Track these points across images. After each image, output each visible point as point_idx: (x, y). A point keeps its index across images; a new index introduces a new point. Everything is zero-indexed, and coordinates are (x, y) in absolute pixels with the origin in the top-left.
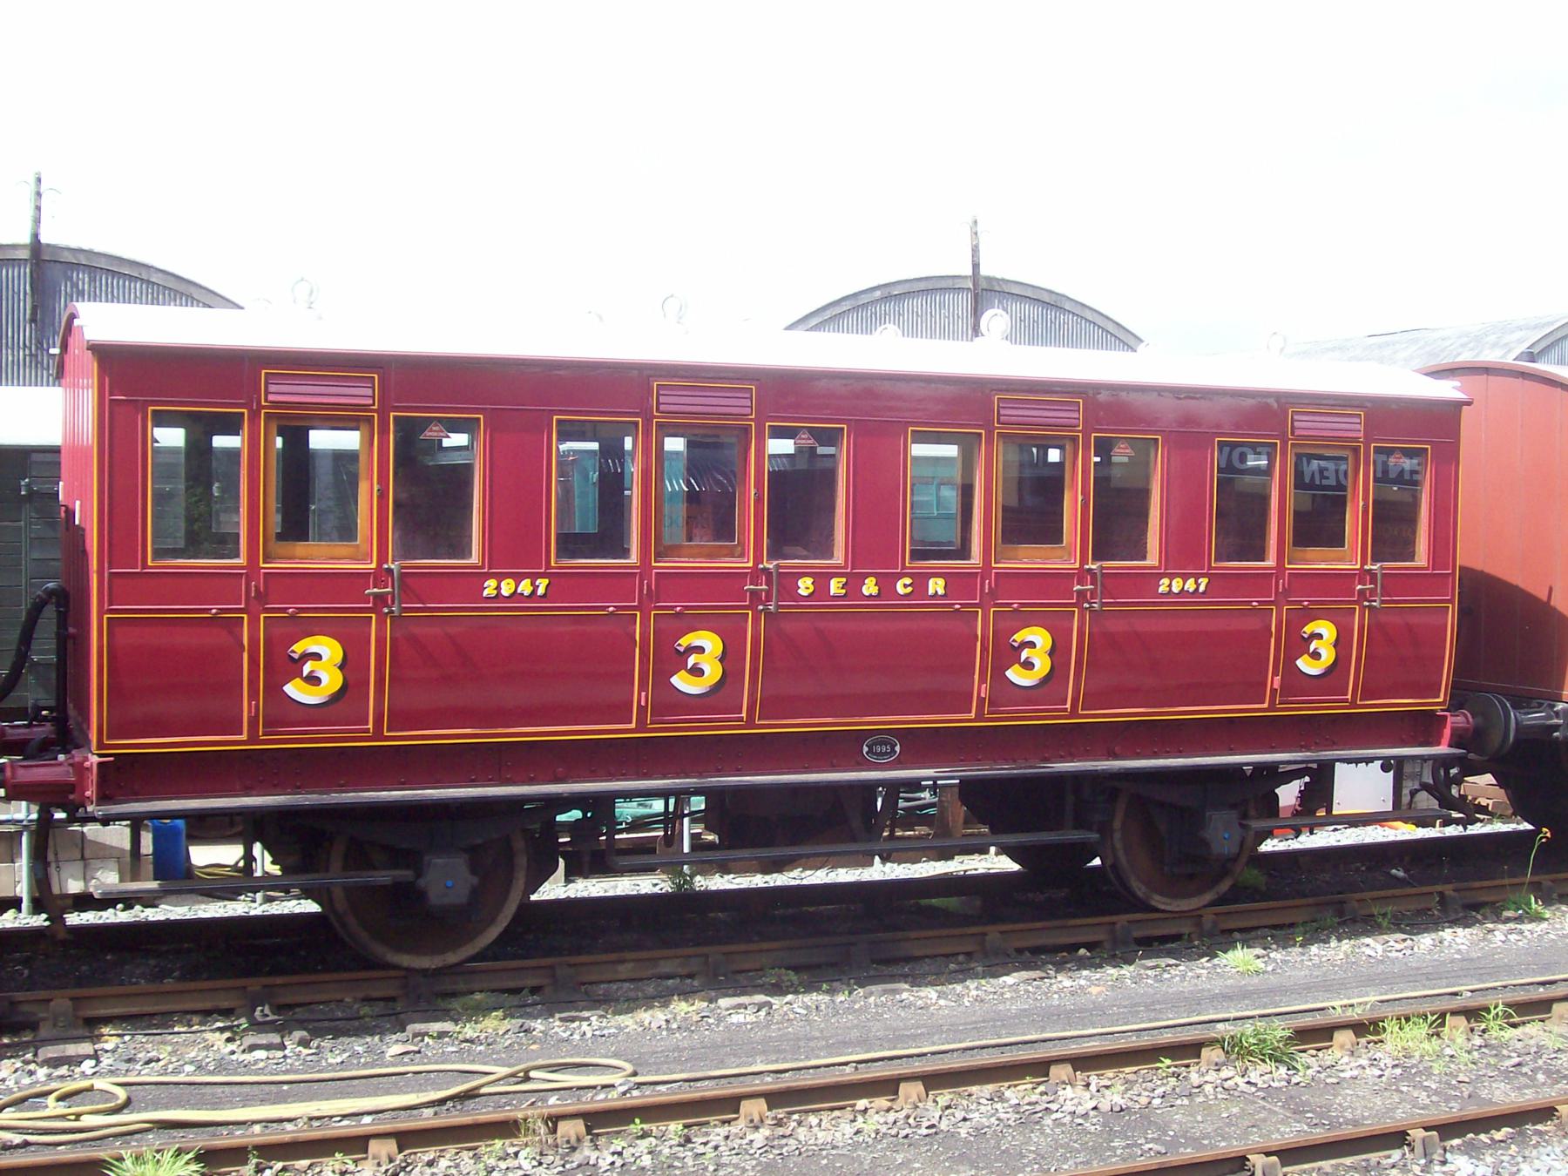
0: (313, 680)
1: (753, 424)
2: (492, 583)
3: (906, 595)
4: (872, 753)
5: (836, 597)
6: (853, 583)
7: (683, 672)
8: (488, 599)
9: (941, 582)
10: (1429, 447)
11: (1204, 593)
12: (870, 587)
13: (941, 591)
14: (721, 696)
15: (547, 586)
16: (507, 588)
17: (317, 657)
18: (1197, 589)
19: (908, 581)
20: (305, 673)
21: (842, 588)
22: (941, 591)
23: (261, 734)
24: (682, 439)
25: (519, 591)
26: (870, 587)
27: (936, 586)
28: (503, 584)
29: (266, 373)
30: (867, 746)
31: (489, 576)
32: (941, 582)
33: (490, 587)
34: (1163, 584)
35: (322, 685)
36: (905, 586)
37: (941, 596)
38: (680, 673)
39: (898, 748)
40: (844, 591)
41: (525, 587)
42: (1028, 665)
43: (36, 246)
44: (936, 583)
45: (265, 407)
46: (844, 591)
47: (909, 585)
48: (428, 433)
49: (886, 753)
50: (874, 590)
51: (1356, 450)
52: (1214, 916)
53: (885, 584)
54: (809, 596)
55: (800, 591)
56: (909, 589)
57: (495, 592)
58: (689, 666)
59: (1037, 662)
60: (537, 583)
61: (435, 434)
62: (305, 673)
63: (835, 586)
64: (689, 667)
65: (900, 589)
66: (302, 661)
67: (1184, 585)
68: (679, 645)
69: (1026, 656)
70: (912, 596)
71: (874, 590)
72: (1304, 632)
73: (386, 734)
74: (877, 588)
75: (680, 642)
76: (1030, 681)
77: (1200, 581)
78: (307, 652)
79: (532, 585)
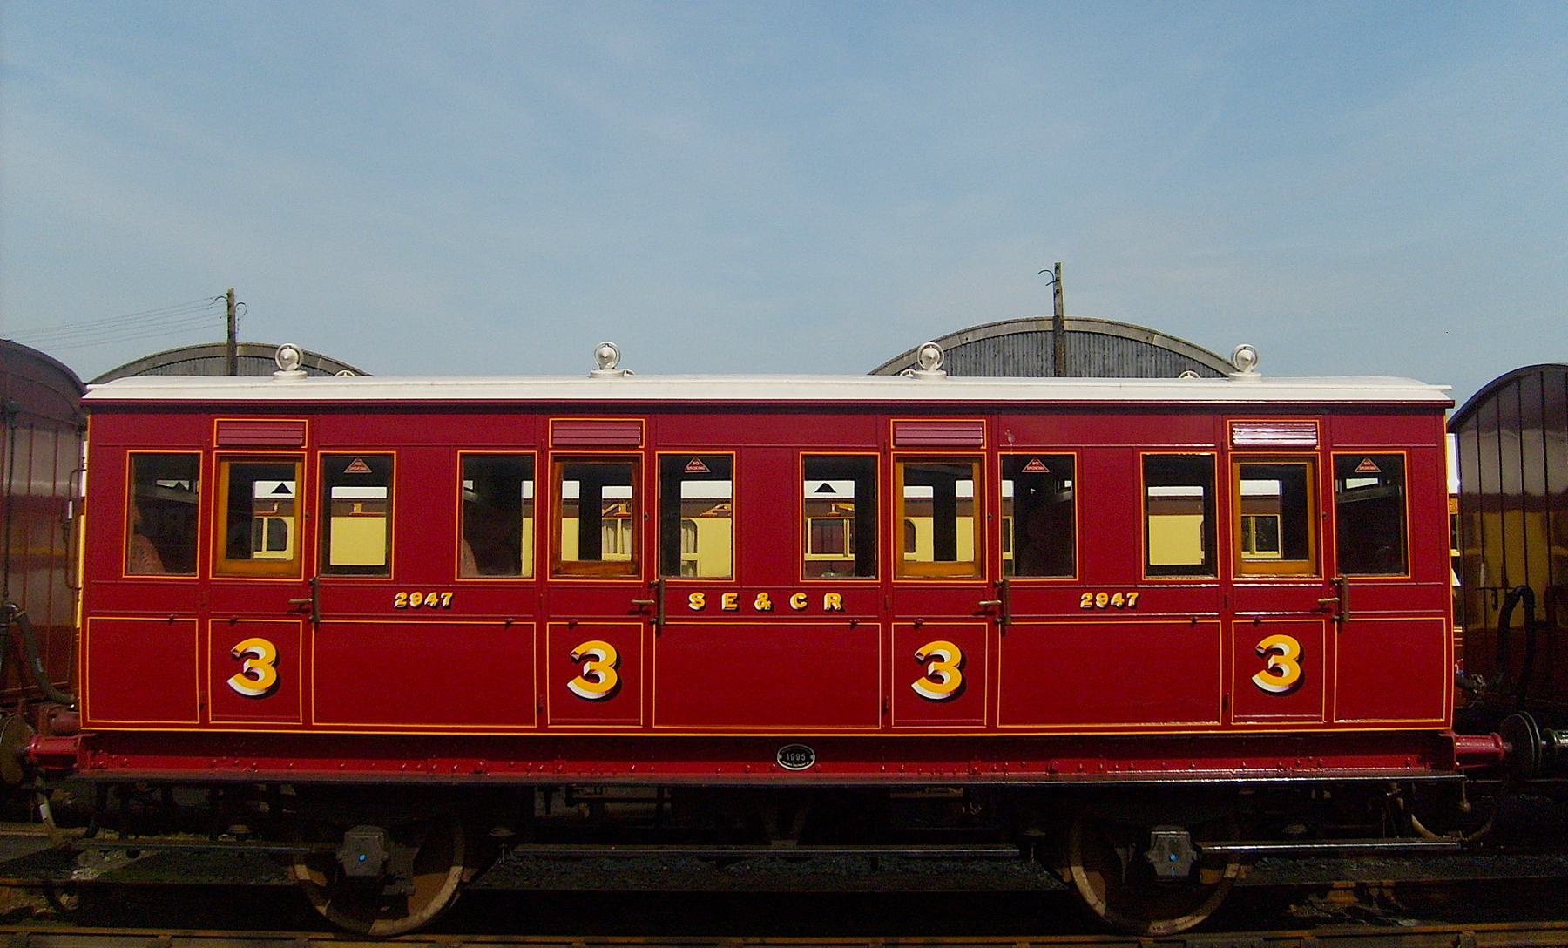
0: (252, 675)
1: (643, 453)
2: (403, 595)
3: (800, 610)
4: (786, 761)
5: (727, 611)
6: (745, 601)
7: (579, 678)
8: (1085, 610)
9: (837, 597)
10: (1405, 453)
11: (1134, 607)
12: (762, 602)
13: (837, 606)
14: (1299, 696)
15: (1137, 598)
16: (416, 599)
17: (255, 656)
18: (439, 603)
19: (802, 596)
20: (1270, 665)
21: (733, 603)
22: (837, 606)
23: (210, 719)
24: (1277, 482)
25: (1112, 602)
26: (762, 602)
27: (832, 601)
28: (1098, 597)
29: (218, 422)
30: (780, 753)
31: (400, 590)
32: (837, 597)
33: (1086, 600)
34: (399, 598)
35: (260, 679)
36: (799, 601)
37: (837, 610)
38: (576, 679)
39: (813, 757)
40: (735, 605)
41: (432, 599)
42: (1276, 671)
43: (1058, 320)
44: (832, 598)
45: (216, 449)
46: (735, 605)
47: (804, 600)
48: (350, 468)
49: (801, 762)
50: (767, 605)
51: (1314, 459)
52: (1474, 933)
53: (780, 601)
54: (701, 609)
55: (690, 605)
56: (803, 604)
57: (405, 603)
58: (585, 673)
59: (946, 676)
60: (442, 596)
61: (1367, 468)
62: (1270, 665)
63: (726, 601)
64: (585, 674)
65: (794, 604)
66: (1268, 656)
67: (424, 600)
68: (575, 653)
69: (1273, 663)
70: (803, 612)
71: (767, 605)
72: (1260, 647)
73: (314, 724)
74: (769, 602)
75: (575, 650)
76: (1281, 687)
77: (1128, 595)
78: (587, 654)
79: (1123, 598)
